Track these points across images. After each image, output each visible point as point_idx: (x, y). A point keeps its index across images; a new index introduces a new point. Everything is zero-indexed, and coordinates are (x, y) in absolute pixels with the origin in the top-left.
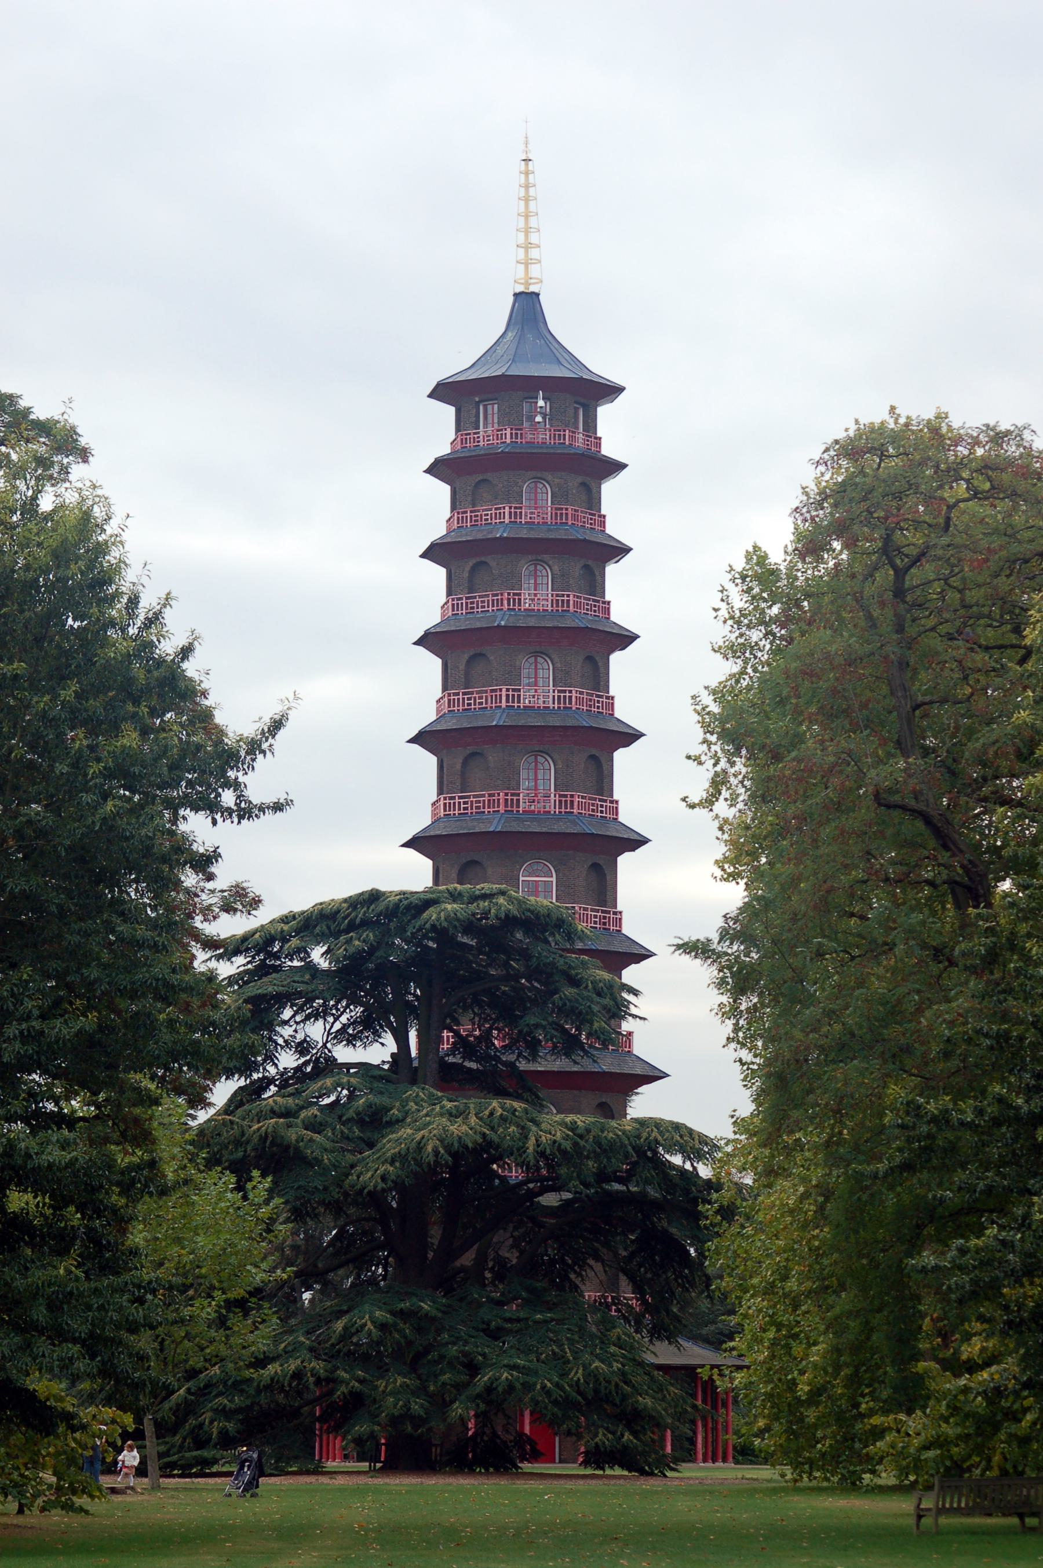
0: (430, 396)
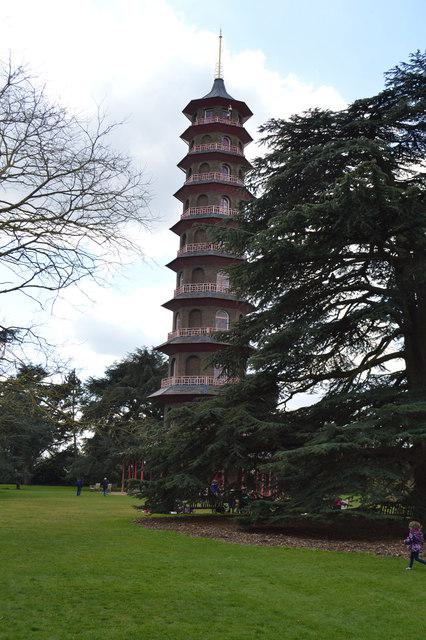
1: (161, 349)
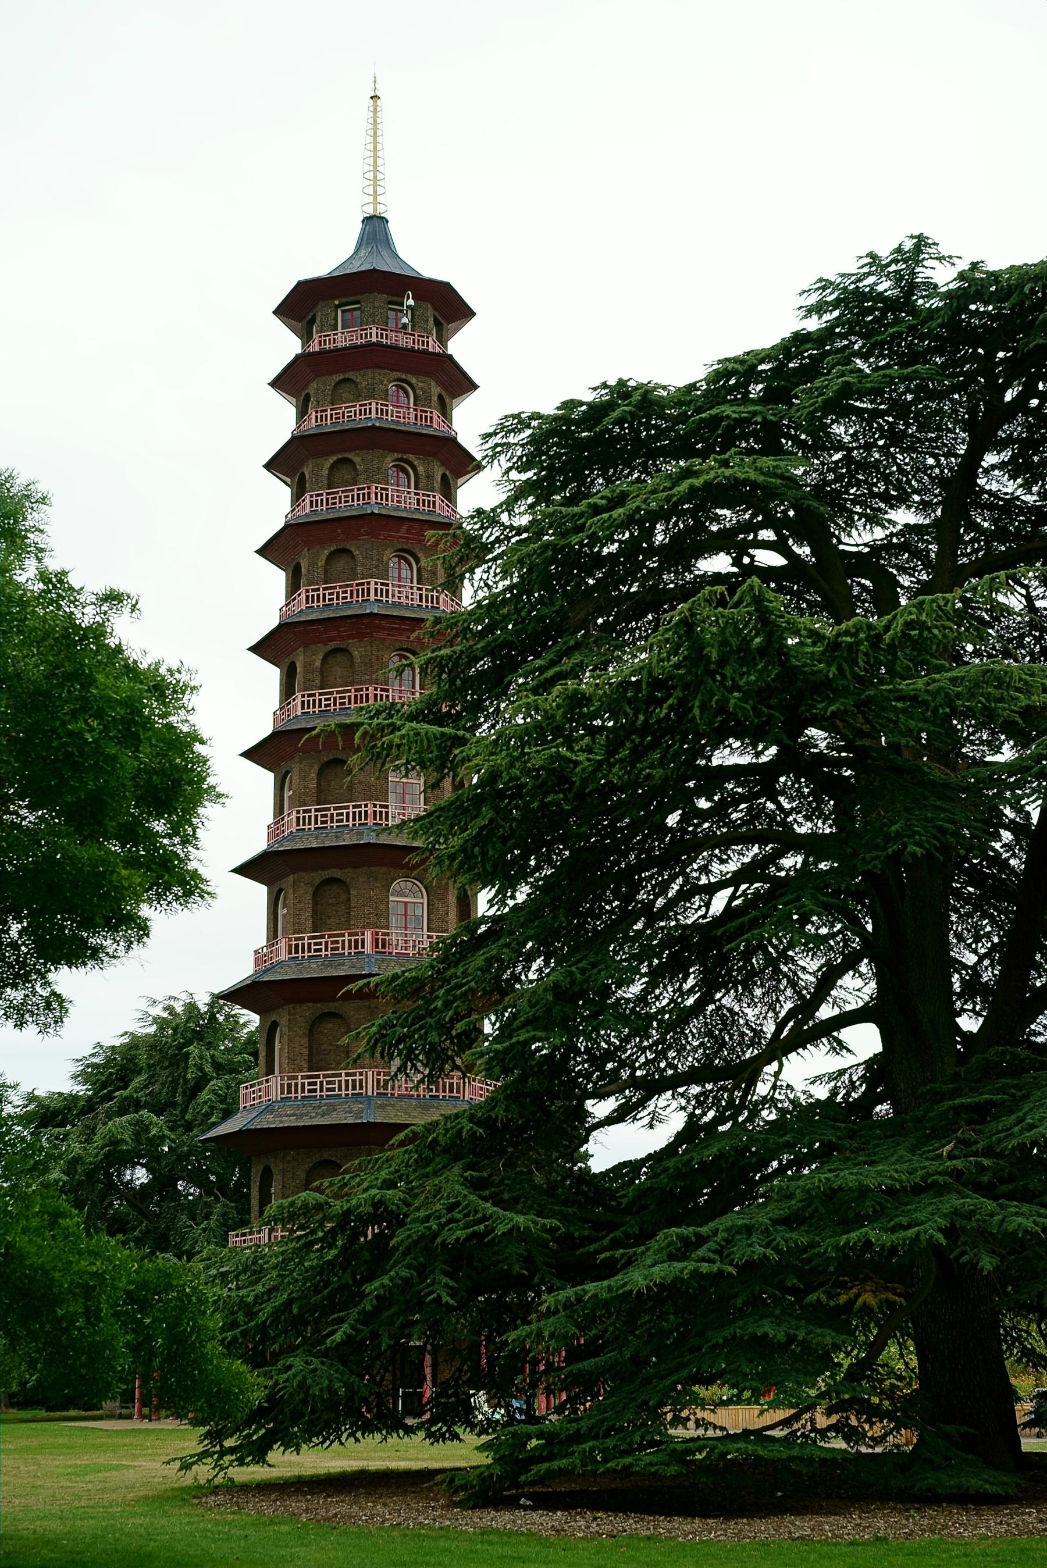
0: (262, 552)
1: (240, 995)
